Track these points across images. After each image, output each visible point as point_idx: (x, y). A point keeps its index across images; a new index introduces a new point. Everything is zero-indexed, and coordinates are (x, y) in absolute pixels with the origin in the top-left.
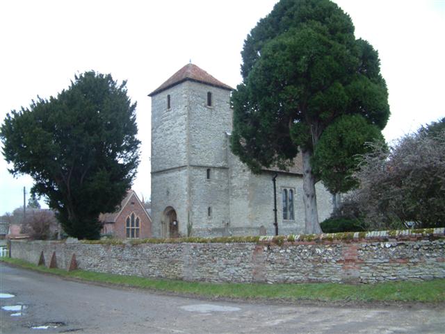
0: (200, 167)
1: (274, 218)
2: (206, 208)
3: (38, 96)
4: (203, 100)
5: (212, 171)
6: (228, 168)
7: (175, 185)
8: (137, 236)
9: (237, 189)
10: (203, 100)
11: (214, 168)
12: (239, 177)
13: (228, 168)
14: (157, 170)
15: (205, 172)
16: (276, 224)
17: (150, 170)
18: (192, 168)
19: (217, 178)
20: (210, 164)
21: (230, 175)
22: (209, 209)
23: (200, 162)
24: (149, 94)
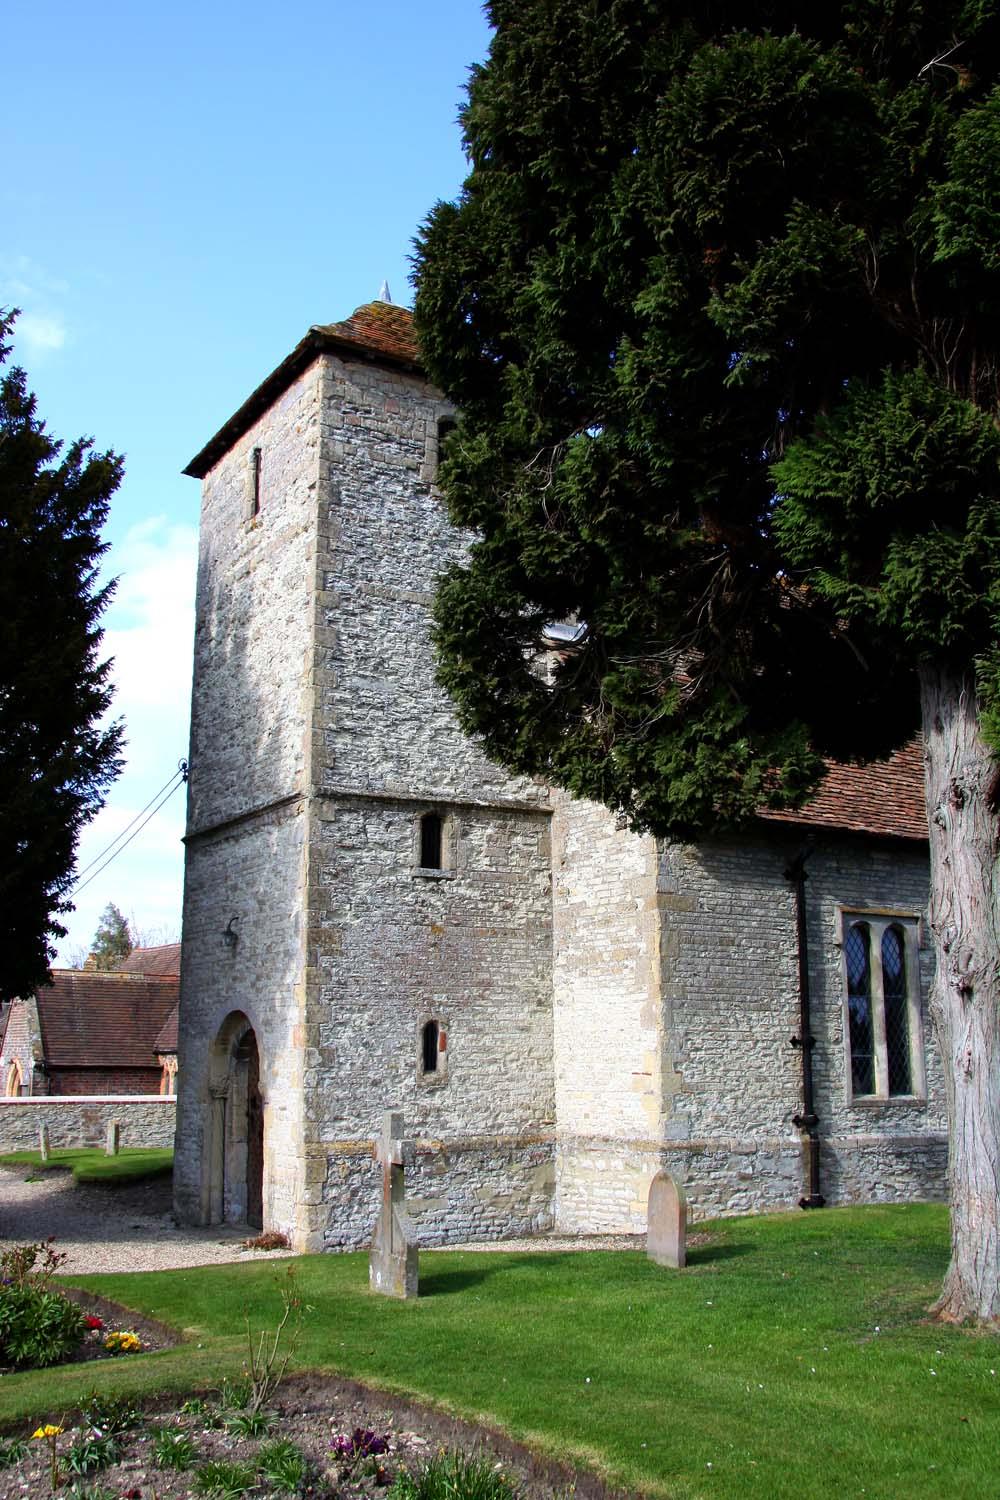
0: (378, 803)
1: (796, 1084)
2: (413, 1028)
3: (112, 658)
4: (412, 459)
5: (450, 826)
6: (549, 814)
7: (261, 903)
8: (167, 1093)
9: (592, 921)
10: (412, 459)
11: (467, 810)
12: (599, 857)
13: (549, 814)
14: (205, 823)
15: (412, 833)
16: (811, 1121)
17: (180, 829)
18: (329, 809)
19: (925, 634)
20: (445, 791)
21: (556, 849)
22: (430, 1033)
23: (388, 780)
24: (184, 468)
